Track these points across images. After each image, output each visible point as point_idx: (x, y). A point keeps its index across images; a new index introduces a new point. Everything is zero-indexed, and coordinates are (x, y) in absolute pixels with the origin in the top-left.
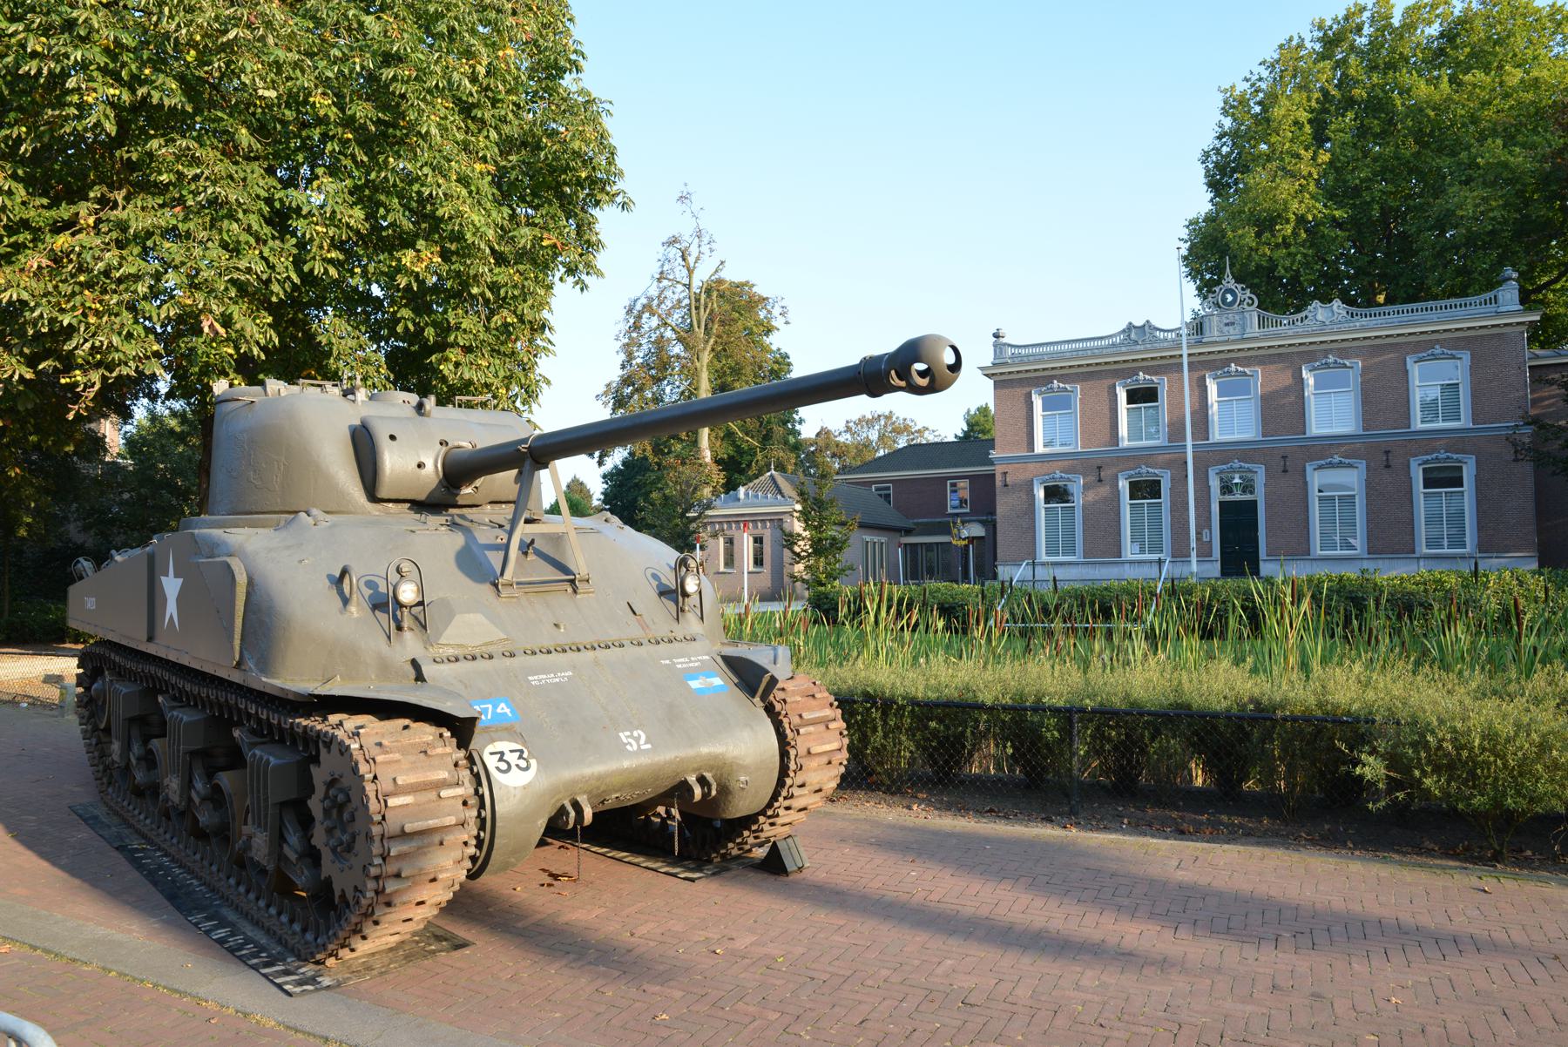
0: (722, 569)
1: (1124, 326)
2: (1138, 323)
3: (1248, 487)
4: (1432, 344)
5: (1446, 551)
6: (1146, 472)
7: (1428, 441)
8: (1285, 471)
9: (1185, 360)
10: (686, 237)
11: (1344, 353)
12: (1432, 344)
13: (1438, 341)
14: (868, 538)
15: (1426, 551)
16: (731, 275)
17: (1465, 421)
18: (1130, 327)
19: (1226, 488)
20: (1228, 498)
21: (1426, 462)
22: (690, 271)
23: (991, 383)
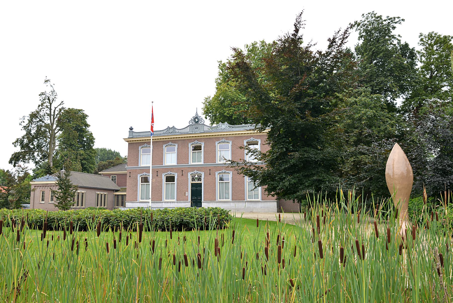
0: (50, 202)
1: (167, 127)
2: (171, 127)
3: (199, 179)
4: (168, 141)
5: (224, 200)
6: (170, 173)
7: (193, 168)
8: (210, 174)
9: (151, 140)
10: (48, 92)
11: (227, 138)
12: (168, 141)
13: (145, 142)
14: (98, 193)
15: (248, 200)
16: (67, 106)
17: (202, 163)
18: (169, 128)
19: (193, 179)
20: (194, 182)
21: (166, 175)
22: (51, 104)
23: (127, 143)
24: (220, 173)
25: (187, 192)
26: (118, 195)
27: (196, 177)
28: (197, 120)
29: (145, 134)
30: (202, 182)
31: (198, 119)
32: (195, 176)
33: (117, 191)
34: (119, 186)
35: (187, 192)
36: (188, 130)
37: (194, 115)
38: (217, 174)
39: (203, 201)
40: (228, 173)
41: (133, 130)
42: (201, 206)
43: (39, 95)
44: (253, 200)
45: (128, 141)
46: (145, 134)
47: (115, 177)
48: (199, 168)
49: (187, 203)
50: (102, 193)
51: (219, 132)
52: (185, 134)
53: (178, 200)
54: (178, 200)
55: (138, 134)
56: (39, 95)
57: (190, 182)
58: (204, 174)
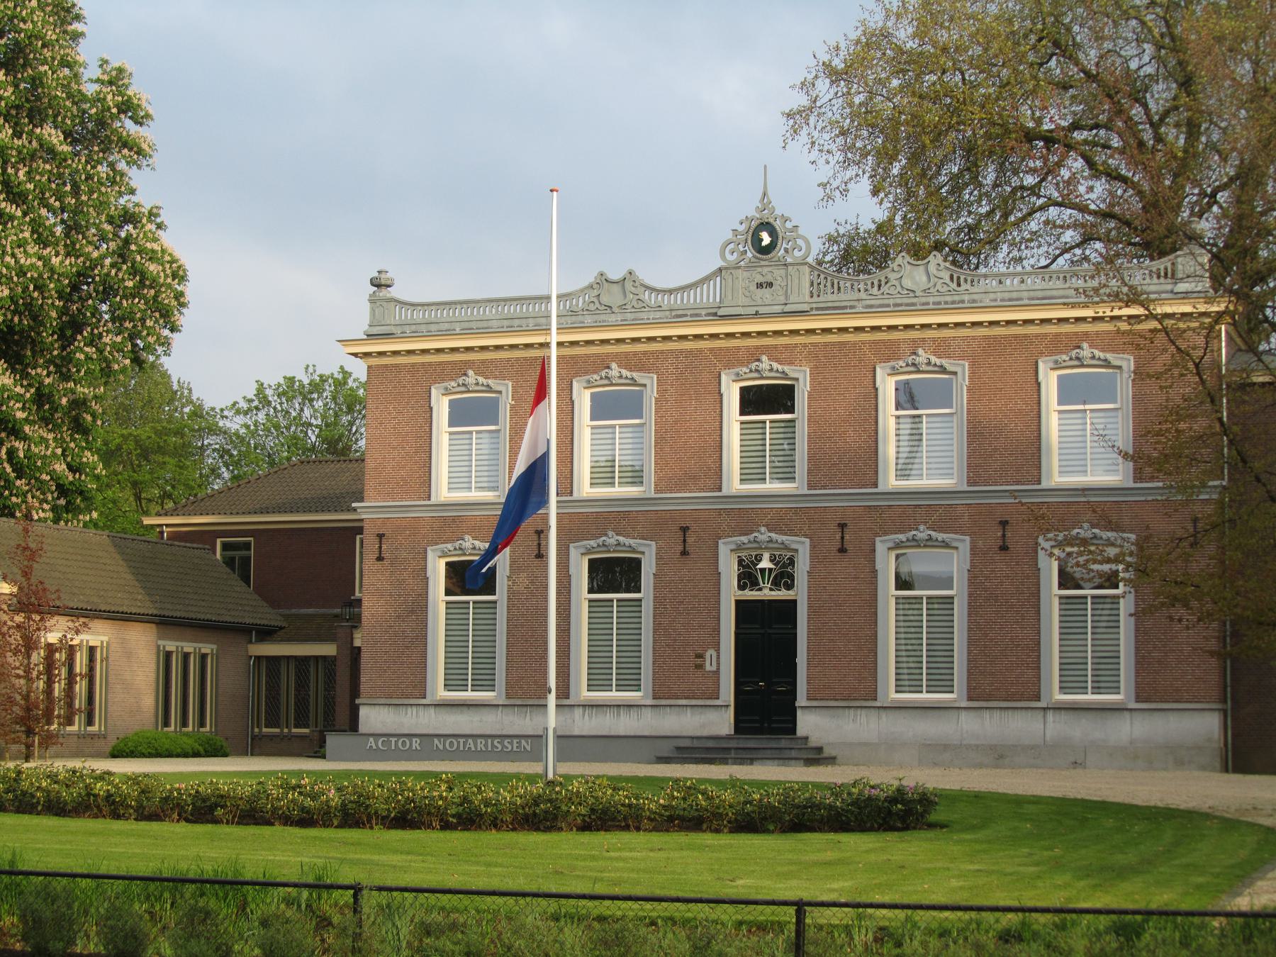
1: (590, 278)
2: (615, 275)
3: (784, 577)
7: (744, 516)
8: (842, 550)
15: (894, 696)
19: (748, 577)
20: (750, 594)
24: (898, 546)
25: (711, 652)
26: (274, 661)
27: (765, 564)
28: (766, 239)
29: (460, 313)
30: (800, 593)
31: (773, 233)
32: (759, 559)
33: (266, 634)
34: (274, 603)
35: (711, 652)
36: (709, 295)
37: (749, 209)
38: (881, 547)
39: (801, 700)
40: (946, 545)
41: (393, 292)
42: (793, 730)
43: (342, 367)
44: (469, 695)
45: (367, 355)
46: (460, 313)
47: (247, 546)
48: (786, 517)
49: (712, 716)
50: (189, 647)
51: (898, 309)
52: (696, 318)
53: (664, 693)
54: (664, 693)
55: (418, 315)
56: (342, 367)
57: (731, 592)
58: (813, 547)
